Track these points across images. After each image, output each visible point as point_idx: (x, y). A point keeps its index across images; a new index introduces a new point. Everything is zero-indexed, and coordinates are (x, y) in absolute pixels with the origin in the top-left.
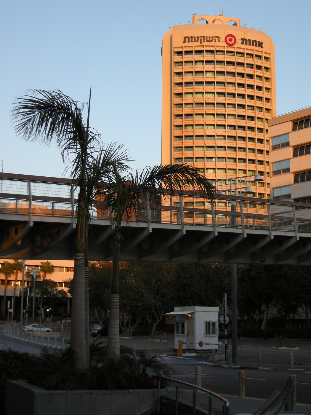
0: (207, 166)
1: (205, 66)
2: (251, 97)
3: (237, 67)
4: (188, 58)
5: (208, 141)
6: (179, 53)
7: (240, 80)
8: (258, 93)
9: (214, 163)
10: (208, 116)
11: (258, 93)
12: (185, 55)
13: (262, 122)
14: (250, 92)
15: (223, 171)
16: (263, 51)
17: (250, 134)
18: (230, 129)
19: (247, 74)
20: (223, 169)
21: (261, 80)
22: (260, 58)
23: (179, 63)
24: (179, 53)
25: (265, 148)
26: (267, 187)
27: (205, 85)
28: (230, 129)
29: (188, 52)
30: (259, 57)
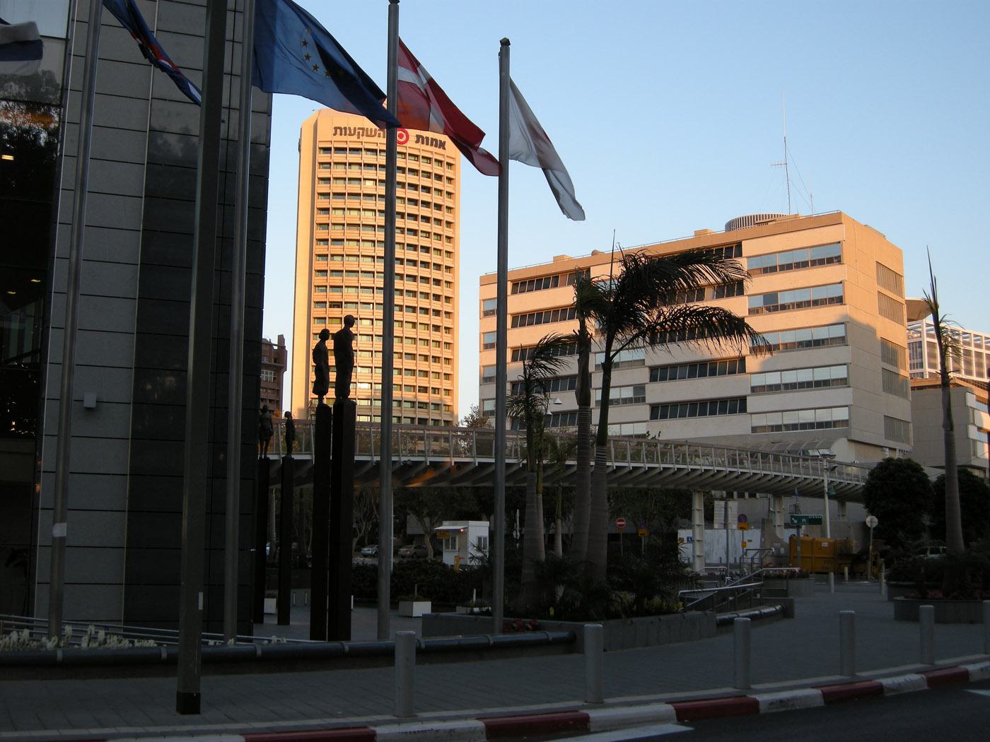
6: (327, 150)
9: (371, 343)
11: (436, 214)
17: (423, 287)
24: (327, 150)
29: (338, 150)
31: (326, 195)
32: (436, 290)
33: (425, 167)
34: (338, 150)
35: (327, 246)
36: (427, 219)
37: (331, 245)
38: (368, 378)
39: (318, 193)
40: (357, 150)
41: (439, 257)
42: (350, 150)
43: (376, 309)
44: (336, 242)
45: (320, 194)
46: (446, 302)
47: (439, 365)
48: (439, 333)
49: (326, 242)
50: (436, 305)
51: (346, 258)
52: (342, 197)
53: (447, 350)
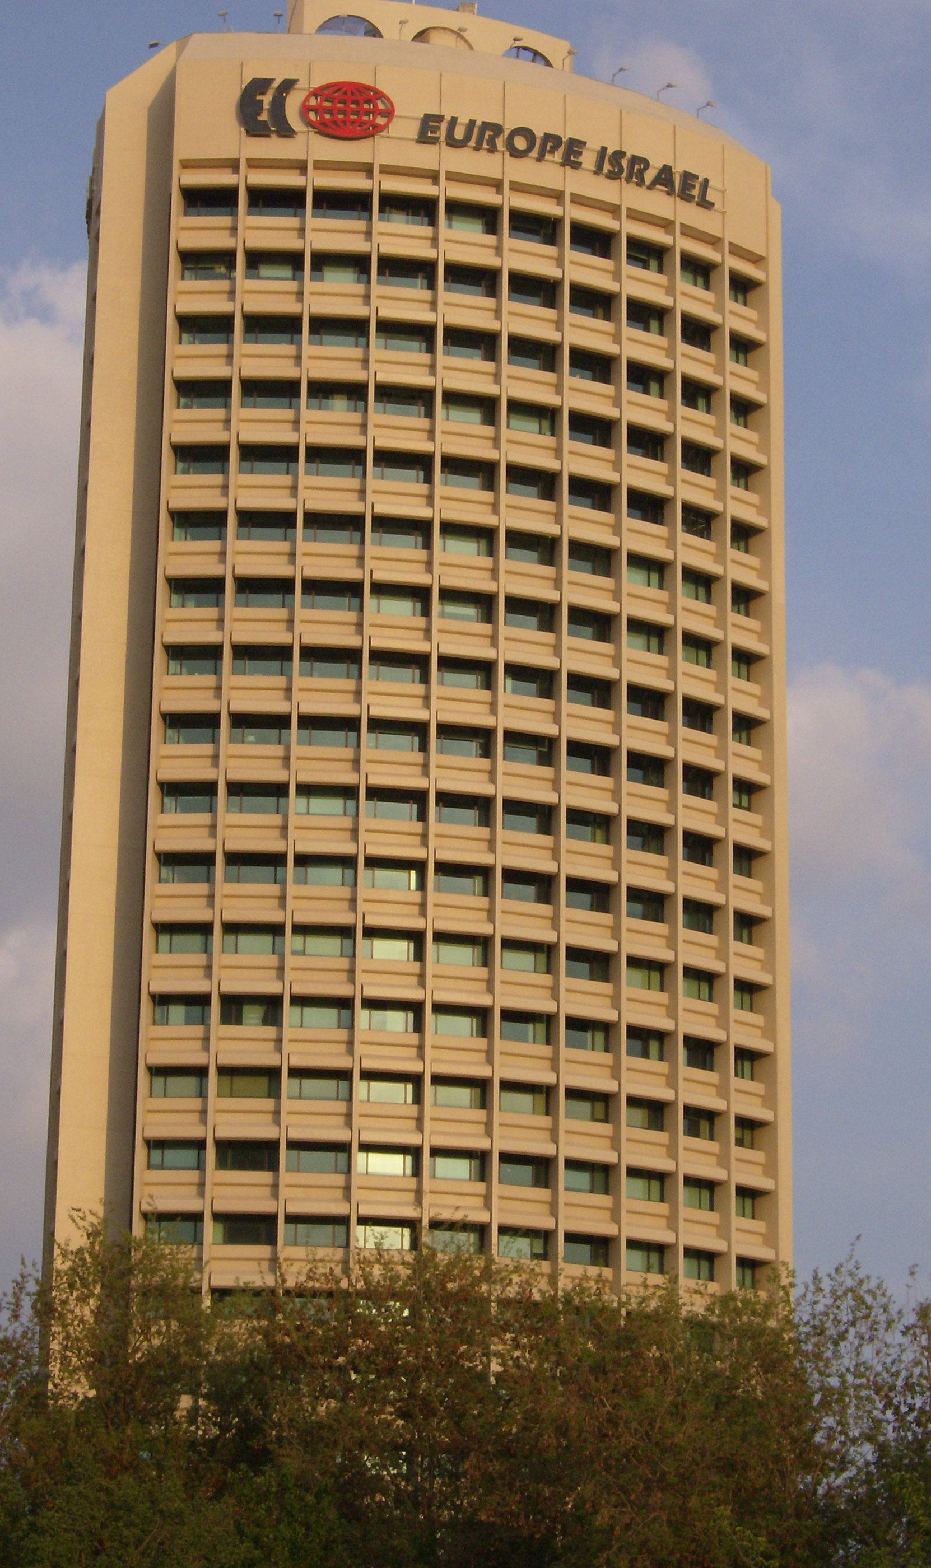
0: (367, 1056)
1: (377, 288)
2: (649, 506)
3: (570, 1121)
4: (269, 230)
5: (382, 686)
6: (201, 199)
7: (587, 396)
8: (692, 488)
9: (417, 897)
10: (382, 668)
11: (692, 488)
12: (242, 406)
13: (712, 1209)
14: (642, 410)
15: (465, 1024)
16: (727, 239)
17: (642, 802)
18: (515, 691)
19: (629, 889)
20: (465, 1226)
21: (708, 666)
22: (705, 987)
23: (194, 792)
24: (201, 199)
25: (724, 564)
26: (736, 1075)
27: (375, 408)
28: (515, 691)
29: (267, 199)
30: (700, 270)
31: (204, 655)
32: (694, 814)
33: (641, 284)
34: (267, 199)
35: (198, 1030)
36: (651, 903)
37: (227, 879)
38: (406, 909)
39: (153, 996)
40: (352, 203)
41: (701, 606)
42: (315, 168)
43: (438, 889)
44: (245, 870)
45: (171, 859)
46: (739, 870)
47: (714, 1146)
48: (712, 940)
49: (197, 1010)
50: (695, 882)
51: (291, 941)
52: (268, 870)
53: (747, 1223)
